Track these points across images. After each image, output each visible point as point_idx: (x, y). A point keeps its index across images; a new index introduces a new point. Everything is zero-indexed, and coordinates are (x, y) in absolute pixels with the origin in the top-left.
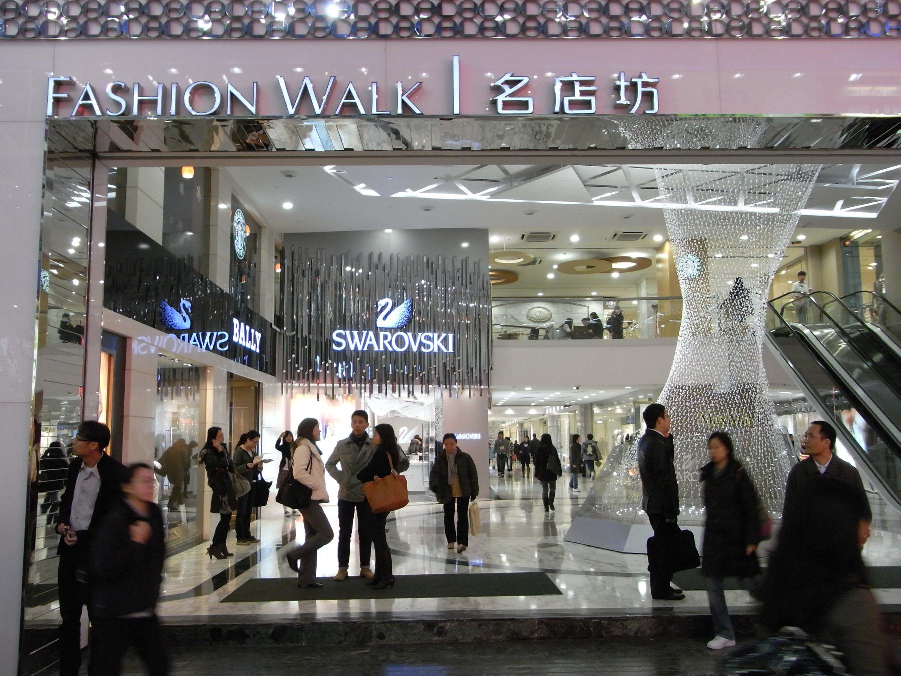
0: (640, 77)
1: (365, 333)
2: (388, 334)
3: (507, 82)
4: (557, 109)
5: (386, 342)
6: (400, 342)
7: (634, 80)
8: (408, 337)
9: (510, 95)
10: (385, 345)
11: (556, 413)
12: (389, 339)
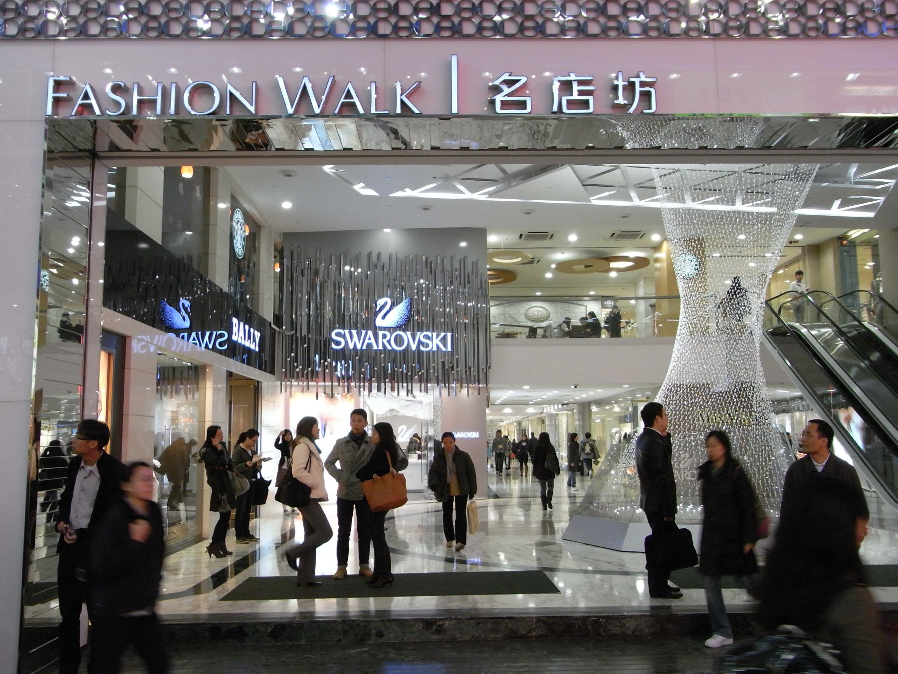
0: (638, 76)
1: (364, 332)
2: (387, 333)
3: (505, 82)
4: (555, 108)
5: (385, 341)
6: (399, 341)
7: (631, 80)
8: (407, 336)
9: (508, 95)
10: (383, 344)
11: (554, 412)
12: (388, 338)
